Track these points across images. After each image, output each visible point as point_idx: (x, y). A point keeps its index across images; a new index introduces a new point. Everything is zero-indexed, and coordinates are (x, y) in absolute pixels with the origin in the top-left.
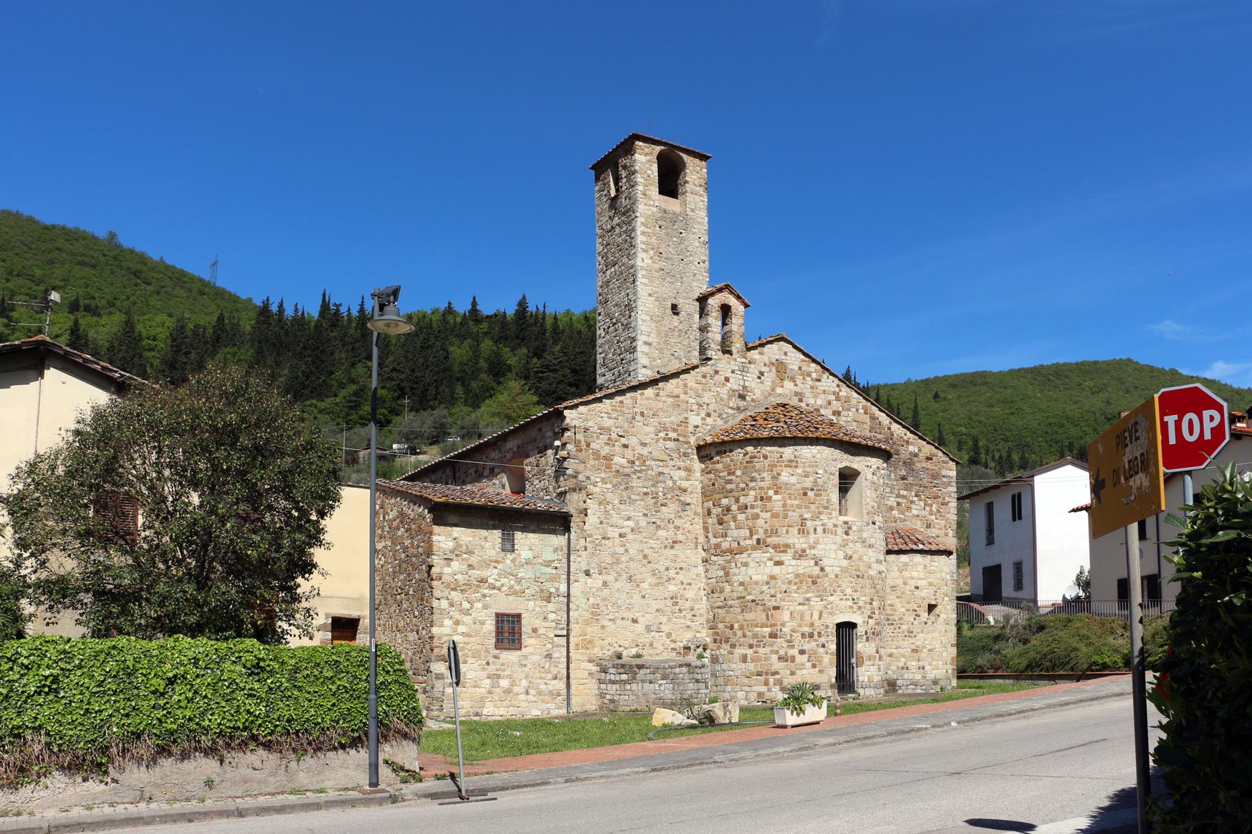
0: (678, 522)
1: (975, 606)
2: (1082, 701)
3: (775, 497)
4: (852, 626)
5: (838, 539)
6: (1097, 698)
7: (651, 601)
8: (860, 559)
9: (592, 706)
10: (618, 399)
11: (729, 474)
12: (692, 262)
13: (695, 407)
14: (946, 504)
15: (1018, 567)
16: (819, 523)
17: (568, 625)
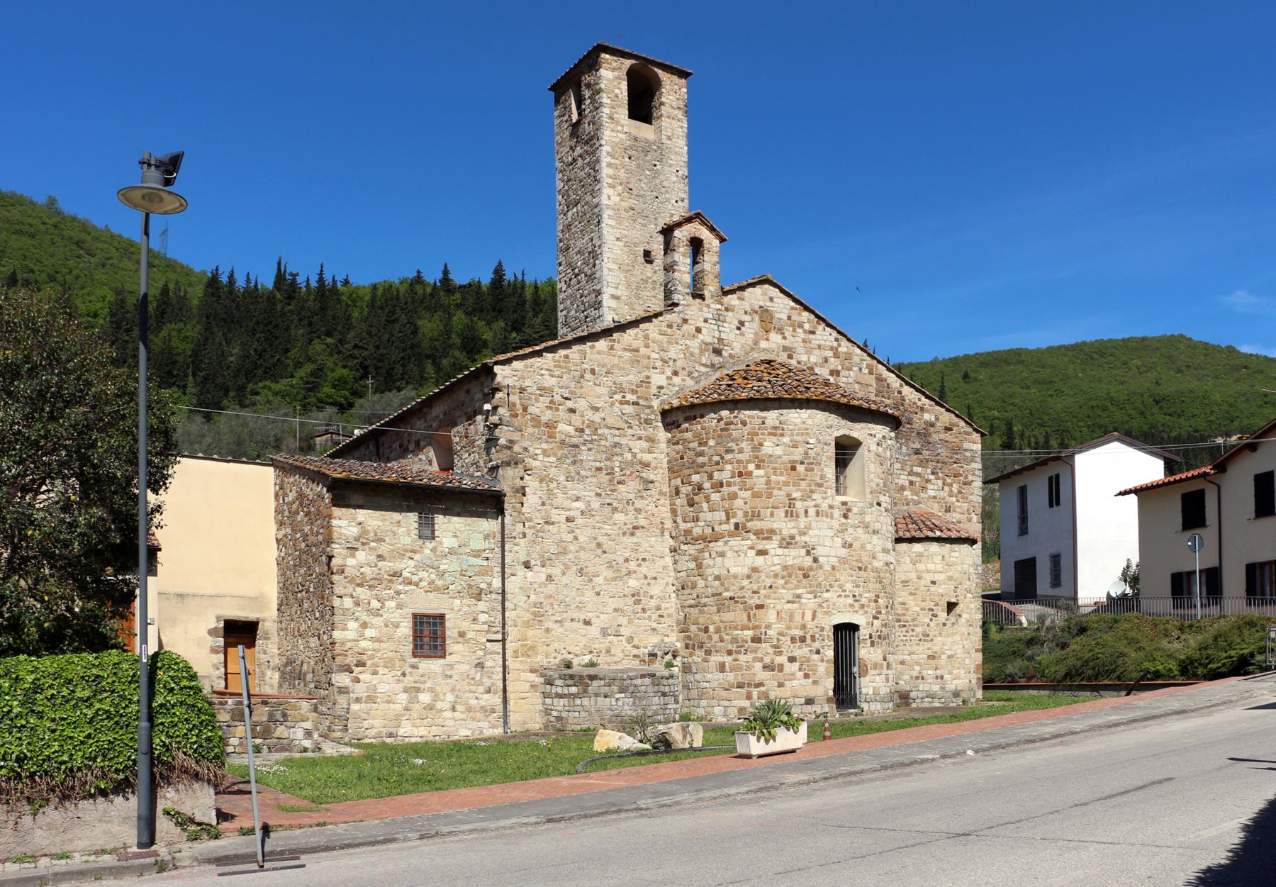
0: (639, 504)
1: (1005, 604)
2: (1135, 721)
3: (757, 473)
4: (854, 628)
5: (835, 524)
6: (1154, 717)
7: (606, 599)
8: (863, 547)
9: (536, 724)
10: (562, 352)
11: (700, 444)
12: (668, 200)
13: (659, 364)
14: (970, 483)
15: (1056, 560)
16: (812, 504)
17: (503, 628)
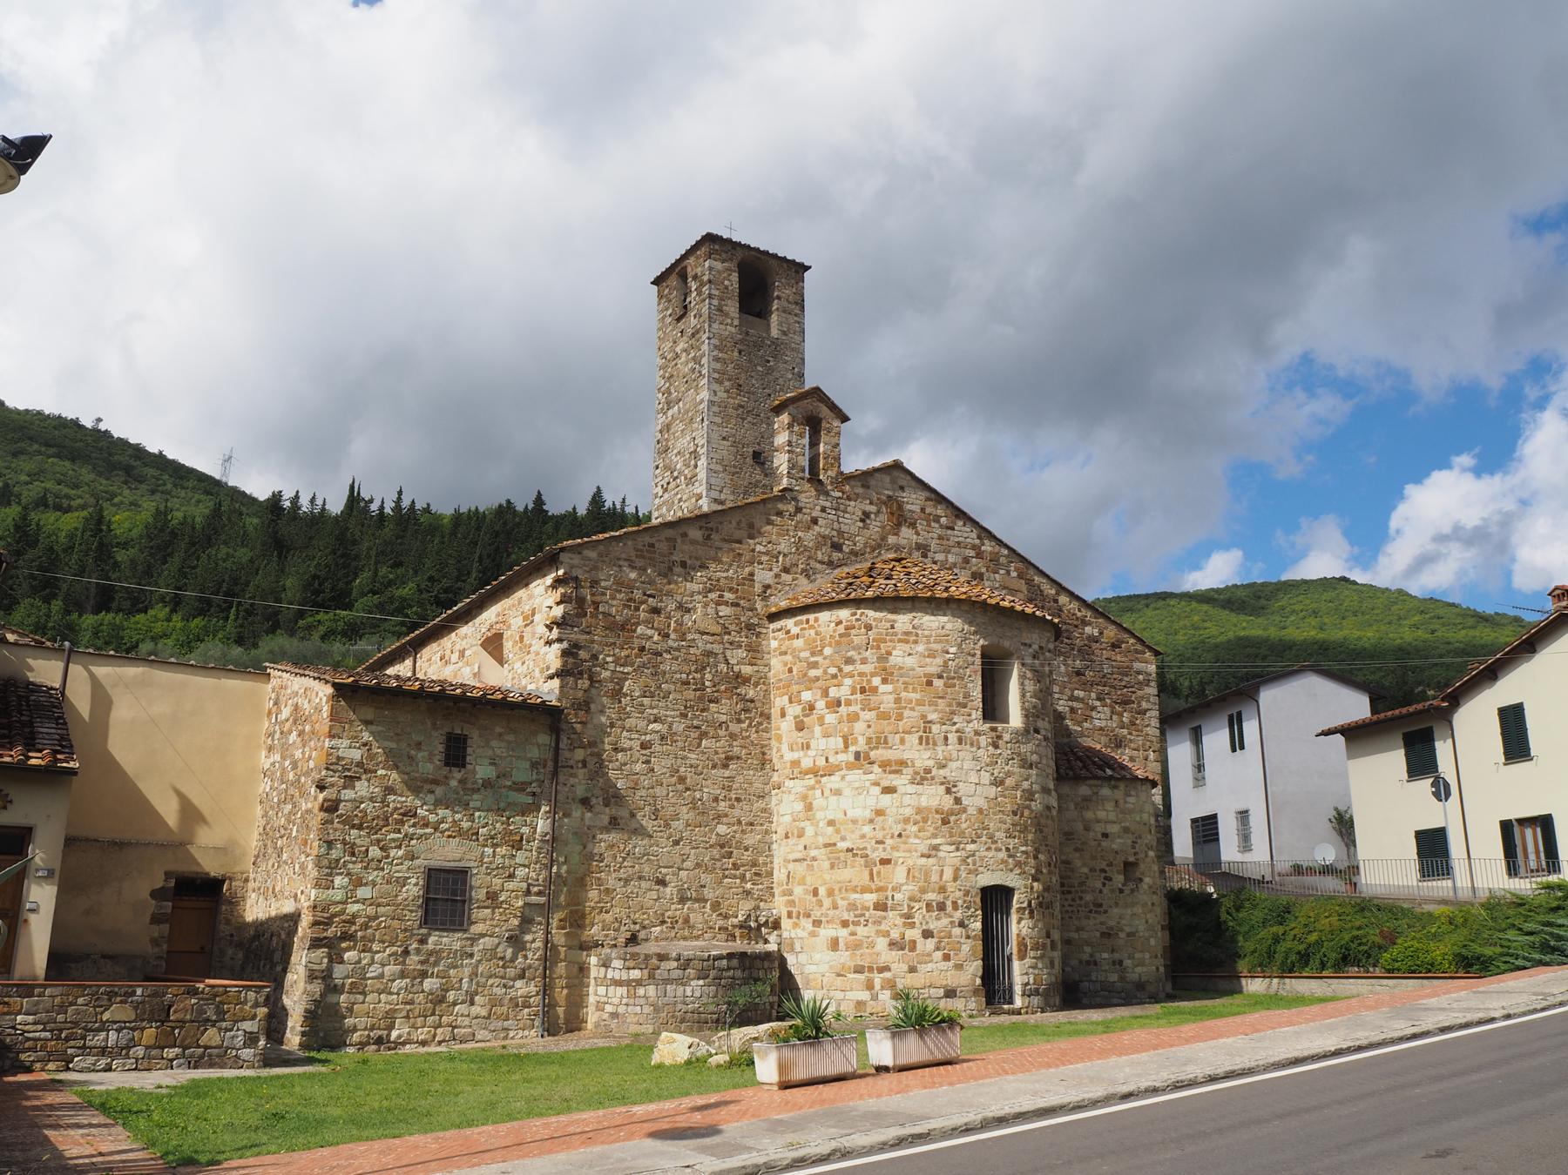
0: (734, 728)
11: (813, 654)
14: (1144, 712)
